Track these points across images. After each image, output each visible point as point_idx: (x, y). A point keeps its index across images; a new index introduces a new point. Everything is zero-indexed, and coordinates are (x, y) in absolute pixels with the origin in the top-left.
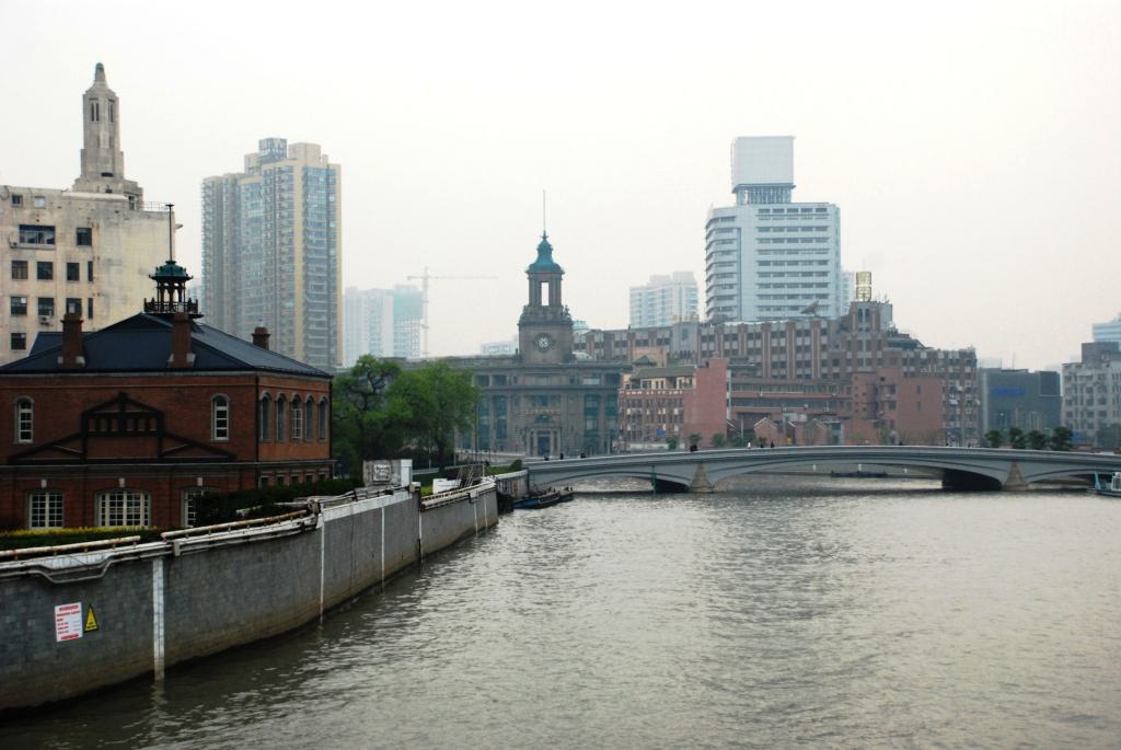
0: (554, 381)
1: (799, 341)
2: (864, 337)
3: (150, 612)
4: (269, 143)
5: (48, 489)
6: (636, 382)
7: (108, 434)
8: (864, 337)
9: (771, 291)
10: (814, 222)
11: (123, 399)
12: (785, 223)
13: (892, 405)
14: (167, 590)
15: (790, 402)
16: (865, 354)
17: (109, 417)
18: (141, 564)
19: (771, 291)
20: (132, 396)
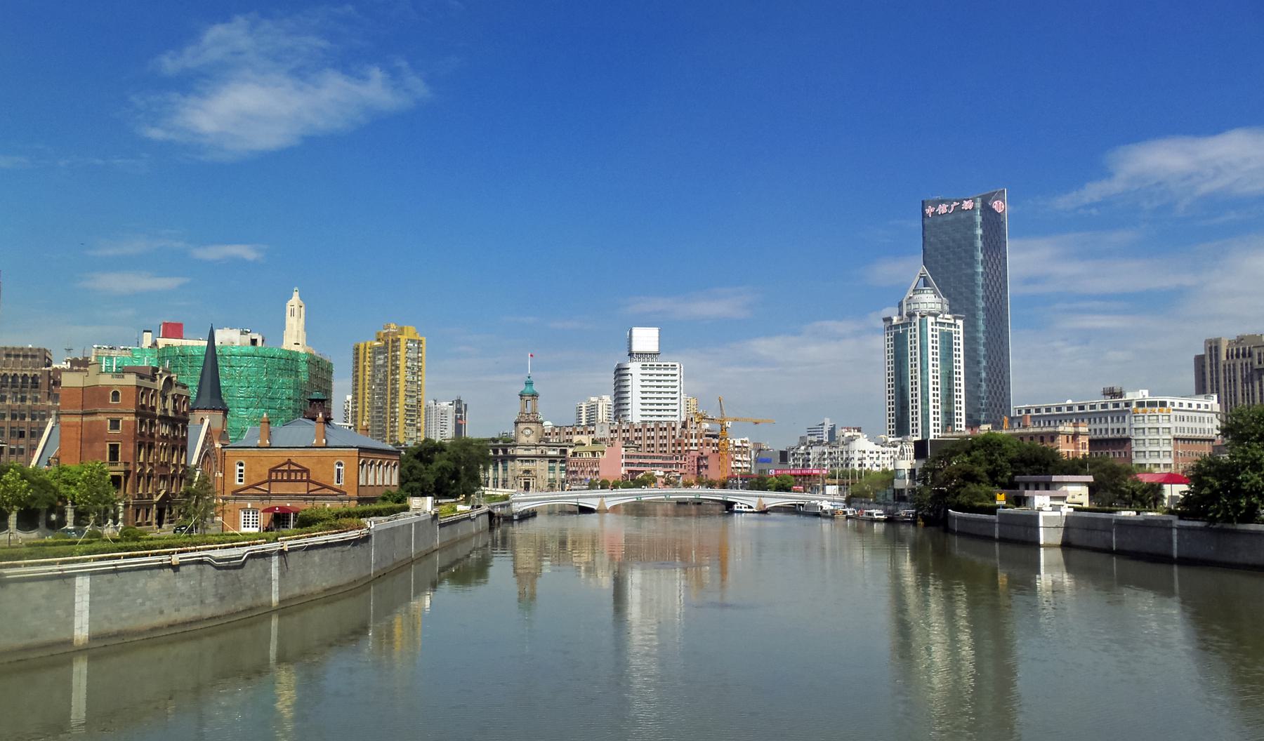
0: (533, 452)
1: (661, 433)
2: (694, 432)
3: (270, 579)
4: (330, 365)
5: (959, 209)
6: (575, 454)
7: (282, 481)
8: (694, 432)
9: (648, 407)
10: (670, 372)
11: (289, 462)
12: (663, 372)
13: (706, 467)
14: (1171, 541)
15: (658, 465)
16: (694, 441)
17: (283, 471)
18: (265, 555)
19: (648, 407)
20: (294, 461)
